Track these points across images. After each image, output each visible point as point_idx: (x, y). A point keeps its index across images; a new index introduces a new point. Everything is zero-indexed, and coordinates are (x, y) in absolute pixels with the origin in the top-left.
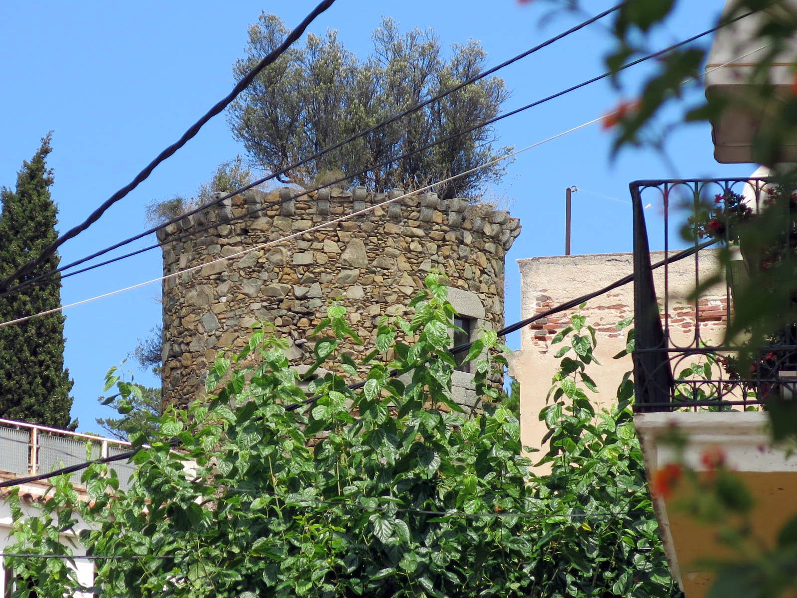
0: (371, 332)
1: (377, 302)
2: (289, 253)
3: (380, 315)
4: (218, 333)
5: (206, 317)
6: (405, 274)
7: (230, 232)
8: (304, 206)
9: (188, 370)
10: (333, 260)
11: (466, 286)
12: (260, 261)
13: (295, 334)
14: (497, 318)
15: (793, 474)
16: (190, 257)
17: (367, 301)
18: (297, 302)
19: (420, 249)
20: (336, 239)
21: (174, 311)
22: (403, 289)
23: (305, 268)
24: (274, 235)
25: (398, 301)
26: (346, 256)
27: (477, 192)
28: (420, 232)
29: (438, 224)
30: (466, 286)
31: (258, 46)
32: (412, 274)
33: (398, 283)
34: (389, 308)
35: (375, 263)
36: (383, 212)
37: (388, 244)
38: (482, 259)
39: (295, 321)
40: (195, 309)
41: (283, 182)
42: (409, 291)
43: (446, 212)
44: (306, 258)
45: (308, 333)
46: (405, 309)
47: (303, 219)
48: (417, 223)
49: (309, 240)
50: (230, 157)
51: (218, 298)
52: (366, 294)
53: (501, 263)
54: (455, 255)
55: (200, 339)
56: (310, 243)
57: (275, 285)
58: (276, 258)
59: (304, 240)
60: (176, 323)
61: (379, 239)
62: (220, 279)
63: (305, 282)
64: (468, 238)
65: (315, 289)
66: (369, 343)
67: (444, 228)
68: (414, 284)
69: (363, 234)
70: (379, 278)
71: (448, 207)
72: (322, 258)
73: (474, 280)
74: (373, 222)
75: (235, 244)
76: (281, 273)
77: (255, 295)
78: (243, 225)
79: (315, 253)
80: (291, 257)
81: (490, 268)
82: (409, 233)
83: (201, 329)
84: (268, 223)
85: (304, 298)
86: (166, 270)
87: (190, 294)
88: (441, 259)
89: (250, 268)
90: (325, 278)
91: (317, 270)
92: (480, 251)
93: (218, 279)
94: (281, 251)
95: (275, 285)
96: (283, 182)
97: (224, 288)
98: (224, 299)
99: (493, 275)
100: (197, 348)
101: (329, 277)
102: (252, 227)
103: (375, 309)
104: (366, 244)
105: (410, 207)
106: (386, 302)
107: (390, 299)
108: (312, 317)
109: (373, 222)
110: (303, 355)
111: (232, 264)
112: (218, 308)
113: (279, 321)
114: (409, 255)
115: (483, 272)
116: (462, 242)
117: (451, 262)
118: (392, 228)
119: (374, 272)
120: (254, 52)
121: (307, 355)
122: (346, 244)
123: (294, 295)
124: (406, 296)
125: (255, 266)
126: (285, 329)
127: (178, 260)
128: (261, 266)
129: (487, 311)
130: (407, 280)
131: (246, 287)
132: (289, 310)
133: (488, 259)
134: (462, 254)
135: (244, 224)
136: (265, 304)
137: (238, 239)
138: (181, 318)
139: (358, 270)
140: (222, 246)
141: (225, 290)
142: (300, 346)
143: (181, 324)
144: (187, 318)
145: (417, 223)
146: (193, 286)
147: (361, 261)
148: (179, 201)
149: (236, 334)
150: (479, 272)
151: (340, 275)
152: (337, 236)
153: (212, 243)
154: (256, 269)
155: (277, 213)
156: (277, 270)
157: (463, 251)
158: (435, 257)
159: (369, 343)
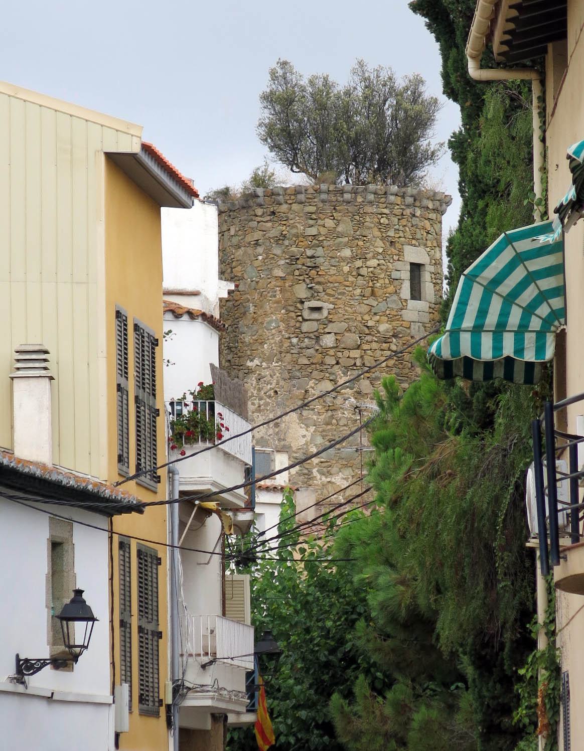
0: (356, 278)
1: (360, 259)
2: (302, 228)
3: (362, 267)
4: (257, 280)
5: (249, 269)
6: (378, 239)
7: (264, 214)
8: (312, 197)
9: (238, 303)
10: (332, 231)
11: (417, 244)
12: (284, 233)
13: (308, 281)
14: (438, 262)
15: (582, 575)
16: (237, 229)
17: (354, 258)
18: (308, 260)
19: (387, 222)
20: (332, 218)
21: (227, 263)
22: (377, 249)
23: (313, 238)
24: (292, 216)
25: (374, 257)
26: (340, 229)
27: (423, 174)
28: (386, 211)
29: (398, 205)
30: (417, 244)
31: (276, 82)
32: (382, 239)
33: (373, 245)
34: (368, 262)
35: (358, 233)
36: (363, 199)
37: (367, 220)
38: (427, 224)
39: (307, 273)
40: (241, 263)
41: (296, 172)
42: (381, 250)
43: (403, 197)
44: (313, 231)
45: (316, 280)
46: (378, 262)
47: (310, 205)
48: (384, 205)
49: (315, 219)
50: (260, 163)
51: (256, 256)
52: (352, 253)
53: (439, 225)
54: (410, 225)
55: (246, 283)
56: (315, 221)
57: (294, 249)
58: (294, 231)
59: (311, 219)
60: (229, 270)
61: (360, 217)
62: (257, 244)
63: (313, 246)
64: (418, 213)
65: (320, 251)
66: (355, 285)
67: (403, 207)
68: (383, 245)
69: (350, 214)
70: (361, 243)
71: (404, 193)
72: (323, 231)
73: (423, 240)
74: (356, 206)
75: (267, 222)
76: (297, 241)
77: (280, 255)
78: (272, 210)
79: (319, 227)
80: (304, 230)
81: (432, 230)
82: (379, 212)
83: (246, 277)
84: (287, 208)
85: (313, 257)
86: (220, 235)
87: (238, 253)
88: (401, 228)
89: (277, 237)
90: (325, 243)
91: (320, 239)
92: (426, 219)
93: (256, 244)
94: (297, 226)
95: (294, 249)
96: (296, 172)
97: (260, 250)
98: (260, 258)
99: (434, 234)
100: (243, 289)
101: (329, 243)
102: (277, 211)
103: (359, 263)
104: (352, 221)
105: (380, 195)
106: (366, 258)
107: (368, 256)
108: (318, 270)
109: (356, 206)
110: (313, 294)
111: (265, 235)
112: (256, 263)
113: (297, 273)
114: (380, 227)
115: (428, 233)
116: (414, 215)
117: (407, 229)
118: (369, 209)
119: (357, 239)
120: (274, 86)
121: (316, 294)
122: (339, 221)
123: (306, 255)
124: (378, 254)
125: (280, 236)
126: (301, 278)
127: (229, 230)
128: (285, 236)
129: (431, 259)
130: (379, 243)
131: (275, 250)
132: (303, 265)
133: (431, 224)
134: (414, 223)
135: (272, 209)
136: (287, 261)
137: (268, 218)
138: (232, 268)
139: (347, 238)
140: (258, 222)
141: (261, 252)
142: (311, 288)
143: (232, 272)
144: (236, 269)
145: (384, 205)
146: (239, 248)
147: (349, 232)
148: (227, 189)
149: (269, 280)
150: (425, 234)
151: (336, 242)
152: (333, 216)
153: (252, 220)
154: (281, 238)
155: (294, 201)
156: (294, 239)
157: (415, 221)
158: (397, 227)
159: (355, 285)
